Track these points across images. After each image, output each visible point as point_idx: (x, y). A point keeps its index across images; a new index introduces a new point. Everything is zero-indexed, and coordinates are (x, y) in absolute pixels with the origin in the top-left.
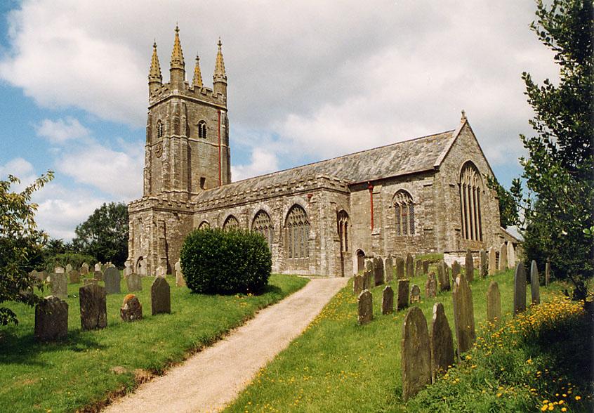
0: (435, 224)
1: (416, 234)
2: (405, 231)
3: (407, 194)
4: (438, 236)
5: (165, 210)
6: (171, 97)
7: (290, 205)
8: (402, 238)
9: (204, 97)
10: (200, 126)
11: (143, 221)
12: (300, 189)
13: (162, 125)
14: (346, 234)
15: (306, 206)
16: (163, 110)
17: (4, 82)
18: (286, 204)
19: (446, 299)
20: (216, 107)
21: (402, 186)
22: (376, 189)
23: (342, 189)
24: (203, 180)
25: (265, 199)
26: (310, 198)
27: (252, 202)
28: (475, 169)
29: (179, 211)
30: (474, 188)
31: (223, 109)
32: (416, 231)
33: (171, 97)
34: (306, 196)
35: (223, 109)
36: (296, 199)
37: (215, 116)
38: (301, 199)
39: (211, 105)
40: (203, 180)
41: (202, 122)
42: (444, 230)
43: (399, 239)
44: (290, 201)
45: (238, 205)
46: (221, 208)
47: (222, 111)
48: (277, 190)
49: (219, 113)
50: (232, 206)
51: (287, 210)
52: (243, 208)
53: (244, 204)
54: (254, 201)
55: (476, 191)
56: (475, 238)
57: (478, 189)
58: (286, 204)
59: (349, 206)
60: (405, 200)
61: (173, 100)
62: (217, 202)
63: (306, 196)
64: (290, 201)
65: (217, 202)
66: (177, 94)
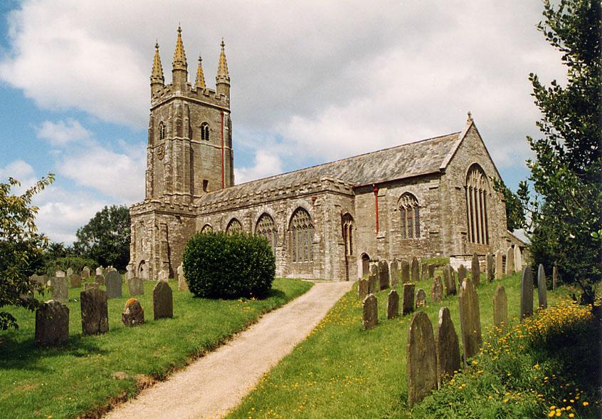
0: (441, 227)
1: (422, 238)
2: (411, 235)
3: (412, 197)
4: (444, 239)
5: (167, 213)
6: (174, 99)
7: (294, 208)
8: (407, 242)
9: (207, 98)
10: (202, 128)
11: (145, 224)
12: (304, 192)
13: (164, 126)
14: (351, 237)
15: (310, 209)
16: (165, 112)
17: (4, 84)
18: (290, 207)
19: (452, 304)
20: (219, 109)
21: (407, 188)
22: (381, 191)
23: (346, 192)
24: (205, 182)
25: (269, 202)
26: (314, 201)
27: (255, 205)
28: (481, 171)
29: (182, 215)
30: (480, 190)
31: (226, 111)
32: (422, 234)
33: (174, 99)
34: (310, 199)
35: (226, 111)
36: (300, 202)
37: (218, 118)
38: (305, 202)
39: (214, 107)
40: (205, 182)
41: (205, 123)
42: (450, 234)
43: (405, 243)
44: (294, 204)
45: (241, 208)
46: (224, 211)
47: (225, 113)
48: (281, 192)
49: (222, 114)
50: (235, 209)
51: (291, 213)
52: (246, 211)
53: (247, 207)
54: (258, 204)
55: (482, 194)
56: (481, 242)
57: (485, 191)
58: (290, 207)
59: (353, 209)
60: (411, 203)
61: (175, 101)
62: (220, 204)
63: (310, 199)
64: (294, 204)
65: (220, 204)
66: (180, 96)
